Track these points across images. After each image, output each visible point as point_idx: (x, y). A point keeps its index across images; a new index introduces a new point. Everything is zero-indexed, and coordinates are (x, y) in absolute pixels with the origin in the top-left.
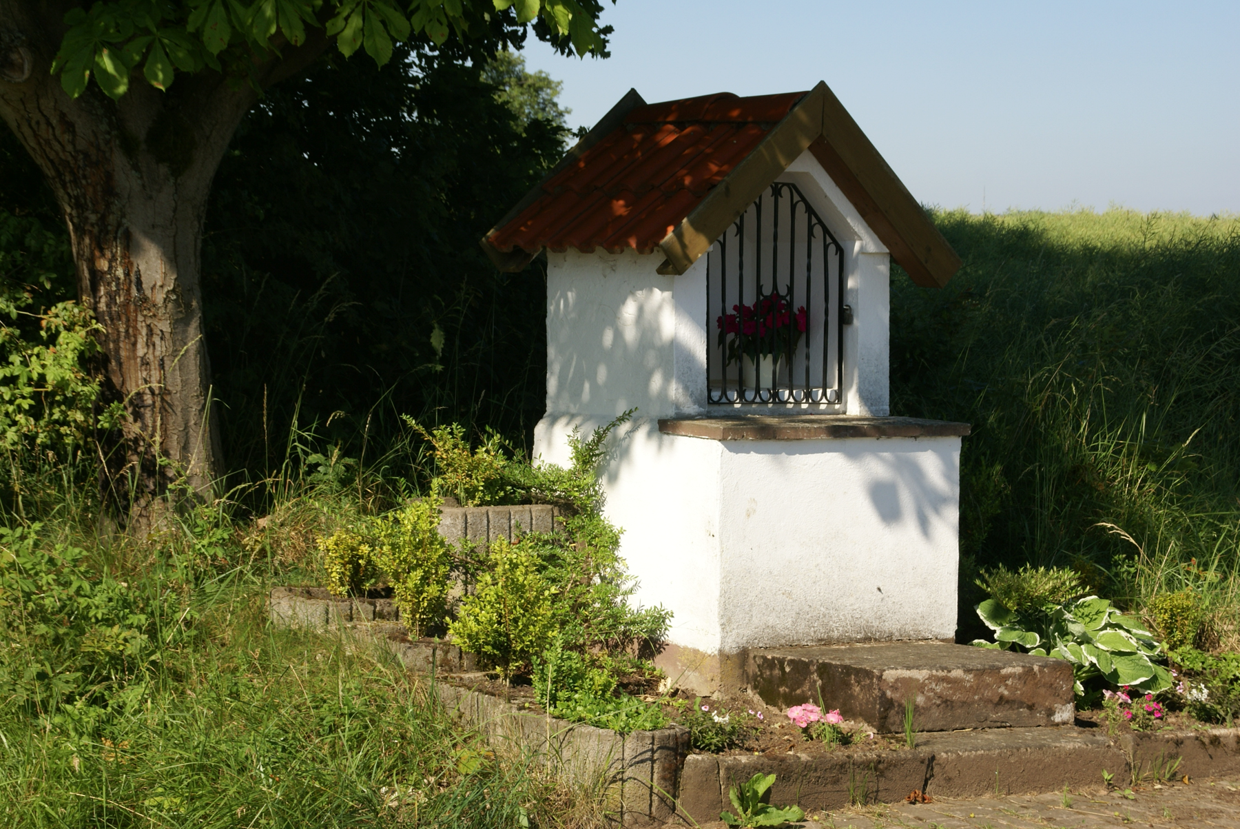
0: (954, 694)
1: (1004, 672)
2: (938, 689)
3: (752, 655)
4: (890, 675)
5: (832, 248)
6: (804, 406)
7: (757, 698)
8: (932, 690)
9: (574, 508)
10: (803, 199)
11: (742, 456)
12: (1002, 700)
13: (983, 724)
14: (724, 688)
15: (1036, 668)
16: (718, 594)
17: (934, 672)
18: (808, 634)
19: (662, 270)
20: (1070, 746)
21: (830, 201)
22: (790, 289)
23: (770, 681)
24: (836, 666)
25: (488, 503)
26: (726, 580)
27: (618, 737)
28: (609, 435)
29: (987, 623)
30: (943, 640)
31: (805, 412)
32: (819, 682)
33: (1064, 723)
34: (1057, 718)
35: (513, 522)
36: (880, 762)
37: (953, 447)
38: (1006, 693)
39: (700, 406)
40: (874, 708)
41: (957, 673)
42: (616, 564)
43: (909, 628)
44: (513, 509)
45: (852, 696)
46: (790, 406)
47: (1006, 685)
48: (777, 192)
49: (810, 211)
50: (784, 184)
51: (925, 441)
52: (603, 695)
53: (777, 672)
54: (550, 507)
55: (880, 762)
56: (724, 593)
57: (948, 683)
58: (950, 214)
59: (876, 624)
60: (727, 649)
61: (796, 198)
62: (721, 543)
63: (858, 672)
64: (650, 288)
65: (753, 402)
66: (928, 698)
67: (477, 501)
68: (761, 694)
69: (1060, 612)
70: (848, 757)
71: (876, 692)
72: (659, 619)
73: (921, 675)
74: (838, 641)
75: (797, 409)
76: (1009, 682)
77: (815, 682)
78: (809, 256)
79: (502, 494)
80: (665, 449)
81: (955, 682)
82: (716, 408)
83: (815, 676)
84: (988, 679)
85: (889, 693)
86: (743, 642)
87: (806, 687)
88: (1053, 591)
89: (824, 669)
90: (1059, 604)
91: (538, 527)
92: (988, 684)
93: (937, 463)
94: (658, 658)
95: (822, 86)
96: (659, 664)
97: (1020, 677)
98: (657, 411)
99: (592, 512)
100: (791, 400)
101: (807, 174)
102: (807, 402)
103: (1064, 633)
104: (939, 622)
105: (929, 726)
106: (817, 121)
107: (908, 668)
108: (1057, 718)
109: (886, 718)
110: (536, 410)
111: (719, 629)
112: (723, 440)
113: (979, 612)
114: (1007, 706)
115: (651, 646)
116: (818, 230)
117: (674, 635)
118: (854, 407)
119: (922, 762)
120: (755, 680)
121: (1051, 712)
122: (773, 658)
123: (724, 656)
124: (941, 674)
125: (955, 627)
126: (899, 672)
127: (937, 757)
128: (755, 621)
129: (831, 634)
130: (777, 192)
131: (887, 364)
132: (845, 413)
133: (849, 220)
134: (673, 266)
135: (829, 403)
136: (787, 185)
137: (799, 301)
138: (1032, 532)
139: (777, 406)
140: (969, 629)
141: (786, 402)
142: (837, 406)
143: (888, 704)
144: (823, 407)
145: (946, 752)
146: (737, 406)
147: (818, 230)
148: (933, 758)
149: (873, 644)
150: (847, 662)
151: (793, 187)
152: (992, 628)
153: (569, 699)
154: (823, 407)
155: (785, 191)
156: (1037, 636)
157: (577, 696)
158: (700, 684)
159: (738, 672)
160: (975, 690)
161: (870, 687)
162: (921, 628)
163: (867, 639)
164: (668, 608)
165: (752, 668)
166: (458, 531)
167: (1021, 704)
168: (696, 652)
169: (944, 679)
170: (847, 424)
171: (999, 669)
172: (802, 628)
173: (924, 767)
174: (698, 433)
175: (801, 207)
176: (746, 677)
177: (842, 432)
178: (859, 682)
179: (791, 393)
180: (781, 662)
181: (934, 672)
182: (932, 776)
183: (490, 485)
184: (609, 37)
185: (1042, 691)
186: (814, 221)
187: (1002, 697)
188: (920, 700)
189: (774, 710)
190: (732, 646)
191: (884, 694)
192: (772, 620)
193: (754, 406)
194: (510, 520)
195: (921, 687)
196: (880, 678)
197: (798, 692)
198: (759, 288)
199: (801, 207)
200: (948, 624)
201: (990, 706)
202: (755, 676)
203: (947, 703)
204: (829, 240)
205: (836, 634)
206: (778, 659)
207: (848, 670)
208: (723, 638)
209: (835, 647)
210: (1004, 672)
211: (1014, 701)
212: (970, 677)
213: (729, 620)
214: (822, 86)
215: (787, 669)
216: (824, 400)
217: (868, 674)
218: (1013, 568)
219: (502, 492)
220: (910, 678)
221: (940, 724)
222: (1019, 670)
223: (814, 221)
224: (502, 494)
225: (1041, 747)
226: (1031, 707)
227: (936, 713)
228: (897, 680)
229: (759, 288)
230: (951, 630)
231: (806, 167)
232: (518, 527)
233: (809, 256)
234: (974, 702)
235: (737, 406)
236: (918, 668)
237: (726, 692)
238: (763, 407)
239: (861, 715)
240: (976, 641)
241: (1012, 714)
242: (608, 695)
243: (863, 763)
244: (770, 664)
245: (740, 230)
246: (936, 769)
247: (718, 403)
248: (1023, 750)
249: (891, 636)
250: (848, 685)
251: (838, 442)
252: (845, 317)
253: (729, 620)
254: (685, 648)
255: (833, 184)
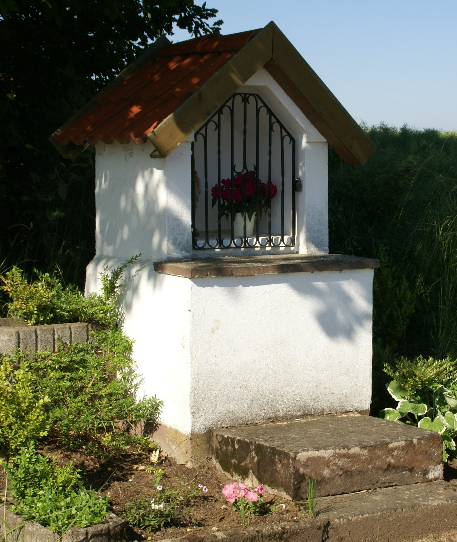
0: (353, 466)
1: (391, 446)
2: (340, 463)
3: (215, 434)
4: (302, 456)
5: (287, 139)
6: (268, 249)
7: (218, 466)
8: (336, 464)
9: (104, 323)
10: (265, 105)
11: (208, 289)
12: (390, 467)
13: (375, 486)
14: (194, 458)
15: (415, 441)
16: (190, 391)
17: (337, 451)
18: (260, 415)
19: (152, 156)
20: (435, 503)
21: (283, 105)
22: (257, 168)
23: (226, 453)
24: (267, 447)
25: (42, 323)
26: (196, 380)
27: (56, 534)
28: (124, 275)
29: (394, 396)
30: (360, 412)
31: (269, 253)
32: (256, 458)
33: (436, 479)
34: (431, 476)
35: (56, 336)
36: (284, 533)
37: (368, 275)
38: (393, 461)
39: (187, 251)
40: (290, 481)
41: (355, 450)
42: (131, 365)
43: (336, 405)
44: (57, 327)
45: (276, 471)
46: (257, 249)
47: (393, 456)
48: (245, 100)
49: (270, 113)
50: (251, 95)
51: (347, 273)
52: (64, 489)
53: (230, 448)
54: (85, 324)
55: (284, 533)
56: (194, 390)
57: (348, 458)
58: (447, 133)
59: (311, 404)
60: (196, 430)
61: (260, 104)
62: (192, 353)
63: (280, 453)
64: (150, 168)
65: (229, 247)
66: (333, 471)
67: (33, 321)
68: (221, 463)
69: (442, 390)
70: (257, 532)
71: (291, 469)
72: (155, 407)
73: (326, 454)
74: (283, 418)
75: (263, 251)
76: (395, 453)
77: (253, 457)
78: (270, 145)
79: (51, 315)
80: (158, 284)
81: (354, 457)
82: (201, 252)
83: (253, 454)
84: (379, 452)
85: (301, 470)
86: (209, 424)
87: (248, 461)
88: (437, 375)
89: (259, 449)
90: (441, 383)
91: (76, 339)
92: (379, 456)
93: (357, 290)
94: (155, 433)
95: (272, 26)
96: (155, 439)
97: (403, 448)
98: (155, 259)
99: (117, 327)
100: (258, 245)
101: (266, 87)
102: (270, 246)
103: (443, 403)
104: (358, 399)
105: (334, 491)
106: (271, 48)
107: (317, 449)
108: (431, 476)
109: (299, 488)
110: (89, 254)
111: (190, 416)
112: (191, 278)
113: (389, 389)
114: (394, 471)
115: (151, 426)
116: (276, 127)
117: (165, 418)
118: (304, 249)
119: (319, 529)
120: (217, 453)
121: (426, 472)
122: (228, 437)
123: (193, 437)
124: (342, 451)
125: (369, 402)
126: (310, 453)
127: (332, 523)
128: (219, 408)
129: (278, 413)
130: (245, 100)
131: (327, 218)
132: (298, 253)
133: (297, 119)
134: (160, 154)
135: (286, 246)
136: (253, 95)
137: (263, 177)
138: (438, 322)
139: (247, 250)
140: (381, 402)
141: (254, 247)
142: (292, 248)
143: (301, 478)
144: (282, 249)
145: (339, 519)
146: (217, 250)
147: (276, 127)
148: (329, 524)
149: (309, 419)
150: (275, 444)
151: (257, 97)
152: (397, 400)
153: (35, 495)
154: (282, 249)
155: (252, 99)
156: (426, 406)
157: (41, 492)
158: (181, 456)
159: (205, 446)
160: (369, 461)
161: (288, 465)
162: (345, 404)
163: (305, 415)
164: (160, 398)
165: (215, 444)
166: (13, 344)
167: (404, 468)
168: (176, 431)
169: (344, 456)
170: (292, 262)
171: (387, 444)
172: (255, 411)
173: (320, 533)
174: (177, 273)
175: (263, 111)
176: (210, 449)
177: (288, 268)
178: (280, 461)
179: (258, 240)
180: (233, 440)
181: (337, 451)
182: (328, 537)
183: (43, 309)
184: (221, 26)
185: (420, 457)
186: (273, 120)
187: (389, 465)
188: (326, 472)
189: (228, 475)
190: (200, 427)
191: (297, 471)
192: (232, 407)
193: (231, 250)
194: (54, 335)
195: (327, 463)
196: (294, 459)
197: (243, 464)
198: (233, 168)
199: (263, 111)
200: (364, 398)
201: (381, 472)
202: (217, 449)
203: (347, 473)
204: (284, 133)
205: (281, 413)
206: (231, 438)
207: (274, 451)
208: (193, 423)
209: (280, 423)
210: (391, 446)
211: (398, 467)
212: (365, 452)
213: (198, 409)
214: (272, 26)
215: (237, 447)
216: (282, 244)
217: (286, 455)
218: (412, 357)
219: (49, 315)
220: (318, 457)
221: (342, 489)
222: (402, 443)
223: (273, 120)
224: (51, 315)
225: (413, 507)
226: (411, 470)
227: (338, 481)
228: (308, 459)
229: (233, 168)
230: (366, 403)
231: (263, 80)
232: (59, 339)
233: (270, 145)
234: (368, 470)
235: (217, 250)
236: (325, 448)
237: (196, 461)
238: (237, 251)
239: (282, 486)
240: (386, 409)
241: (397, 476)
242: (68, 489)
243: (269, 535)
244: (226, 441)
245: (218, 126)
246: (331, 532)
247: (202, 249)
248: (399, 510)
249: (322, 413)
250: (274, 463)
251: (282, 276)
252: (297, 186)
253: (198, 409)
254: (170, 428)
255: (285, 94)
